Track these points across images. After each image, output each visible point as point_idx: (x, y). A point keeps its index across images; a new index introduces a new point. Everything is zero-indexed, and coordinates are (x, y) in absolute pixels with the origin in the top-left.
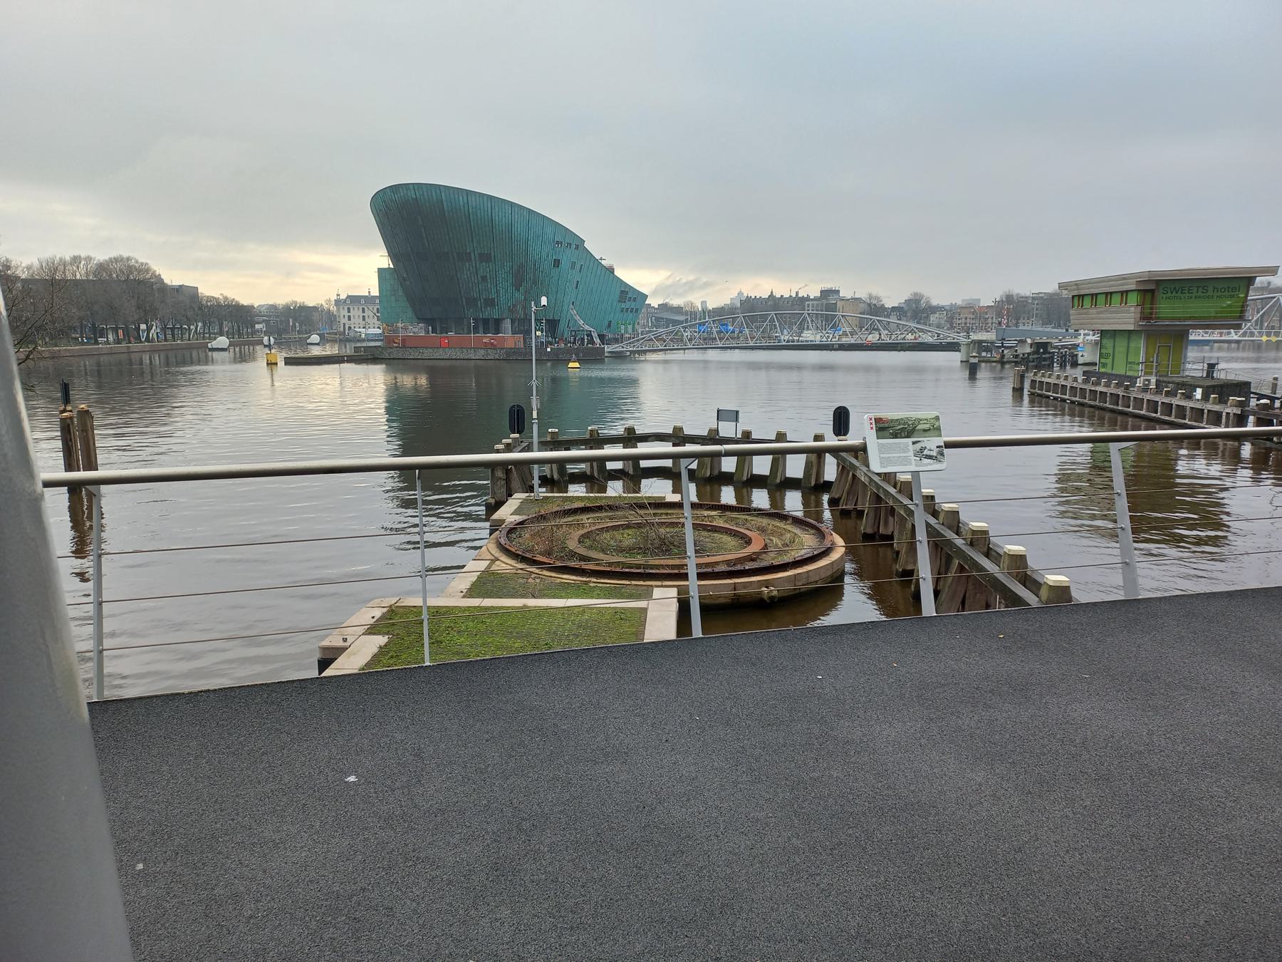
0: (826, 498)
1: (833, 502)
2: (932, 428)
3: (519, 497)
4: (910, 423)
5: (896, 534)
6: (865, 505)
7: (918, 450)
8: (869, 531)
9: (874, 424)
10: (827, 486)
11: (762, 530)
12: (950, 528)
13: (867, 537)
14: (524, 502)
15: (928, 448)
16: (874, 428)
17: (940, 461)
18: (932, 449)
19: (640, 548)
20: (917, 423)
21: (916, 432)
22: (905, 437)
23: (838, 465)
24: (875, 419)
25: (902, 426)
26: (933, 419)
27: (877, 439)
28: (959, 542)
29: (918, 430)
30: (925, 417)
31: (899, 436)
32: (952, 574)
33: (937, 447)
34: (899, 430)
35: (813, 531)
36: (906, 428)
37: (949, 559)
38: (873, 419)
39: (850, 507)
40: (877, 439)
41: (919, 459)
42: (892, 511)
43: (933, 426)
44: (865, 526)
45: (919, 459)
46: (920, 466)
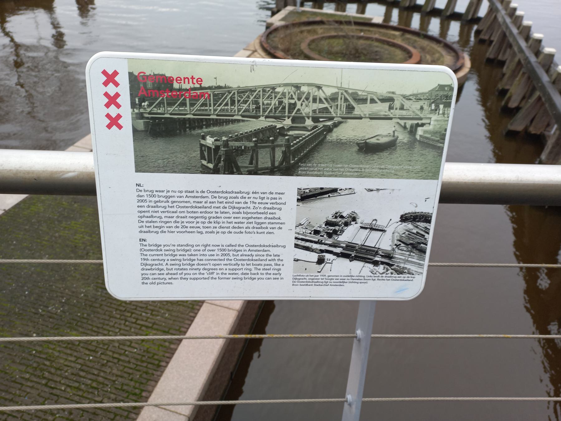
0: (475, 27)
1: (478, 33)
2: (403, 137)
3: (290, 8)
4: (307, 109)
5: (508, 62)
6: (495, 38)
7: (319, 223)
8: (492, 56)
9: (125, 100)
10: (477, 20)
11: (423, 49)
12: (543, 66)
13: (490, 61)
14: (291, 13)
15: (364, 218)
16: (127, 121)
17: (400, 272)
18: (381, 223)
19: (343, 53)
20: (337, 112)
21: (324, 154)
22: (272, 171)
23: (489, 6)
24: (133, 79)
25: (262, 123)
26: (417, 97)
27: (139, 168)
28: (545, 78)
29: (341, 144)
30: (383, 91)
31: (243, 161)
32: (532, 100)
33: (404, 219)
34: (248, 137)
35: (453, 54)
36: (282, 132)
37: (534, 90)
38: (123, 80)
39: (486, 37)
40: (139, 168)
41: (314, 257)
42: (510, 46)
43: (413, 131)
44: (490, 53)
45: (314, 257)
46: (314, 282)
